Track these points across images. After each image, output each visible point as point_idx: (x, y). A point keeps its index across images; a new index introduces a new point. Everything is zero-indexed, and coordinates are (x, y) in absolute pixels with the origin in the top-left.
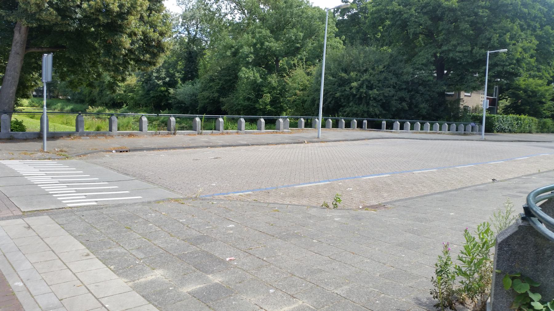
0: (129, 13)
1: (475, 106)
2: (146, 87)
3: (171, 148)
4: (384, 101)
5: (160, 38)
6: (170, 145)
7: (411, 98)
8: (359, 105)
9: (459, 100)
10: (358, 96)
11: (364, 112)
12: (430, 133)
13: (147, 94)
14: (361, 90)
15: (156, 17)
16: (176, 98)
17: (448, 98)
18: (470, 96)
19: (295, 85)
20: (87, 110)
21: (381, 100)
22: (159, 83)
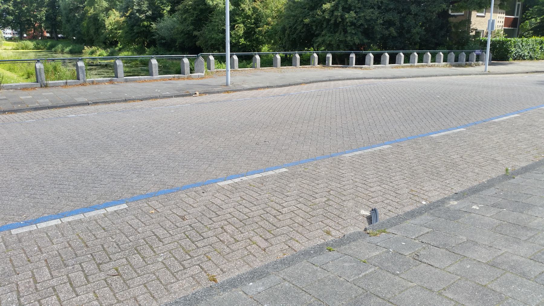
4: (366, 26)
7: (403, 20)
8: (335, 32)
9: (468, 21)
10: (332, 22)
11: (341, 42)
12: (417, 67)
14: (336, 13)
17: (451, 19)
18: (484, 17)
19: (268, 12)
20: (83, 51)
21: (362, 25)
22: (141, 17)
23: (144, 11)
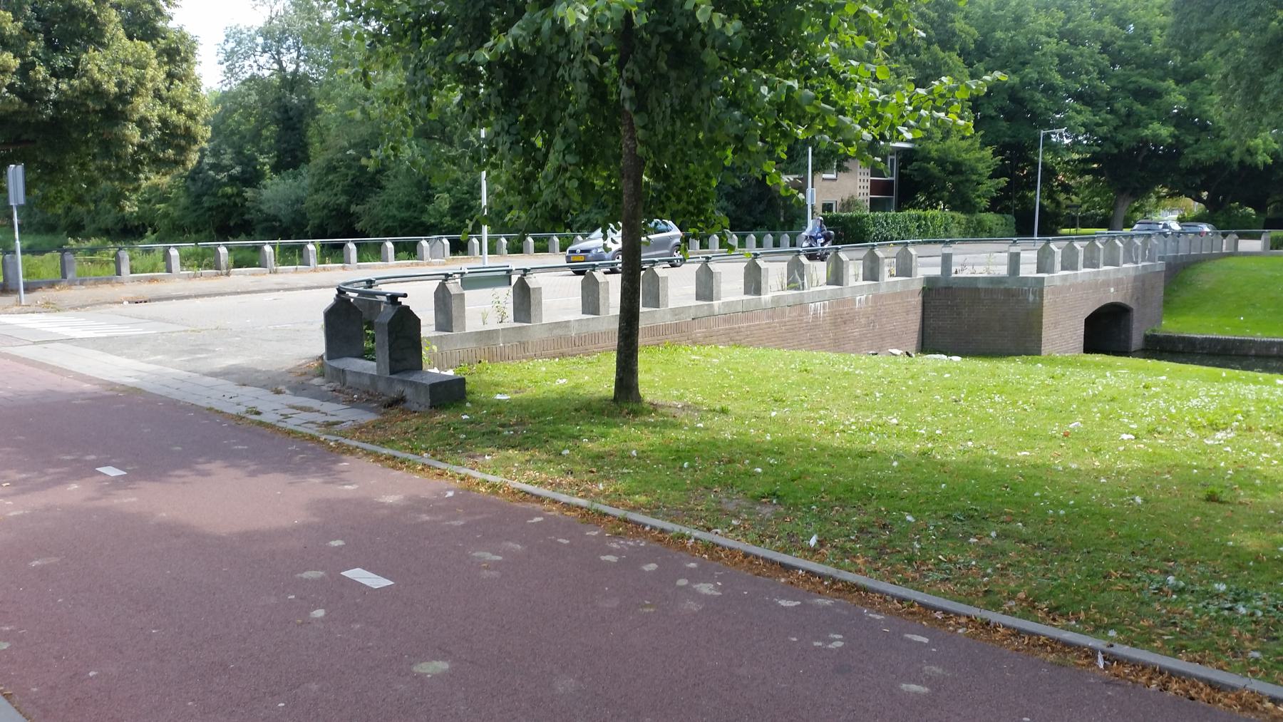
0: (134, 92)
1: (846, 198)
2: (193, 189)
3: (216, 295)
5: (189, 123)
6: (216, 291)
13: (197, 203)
15: (181, 90)
16: (260, 210)
23: (226, 166)
